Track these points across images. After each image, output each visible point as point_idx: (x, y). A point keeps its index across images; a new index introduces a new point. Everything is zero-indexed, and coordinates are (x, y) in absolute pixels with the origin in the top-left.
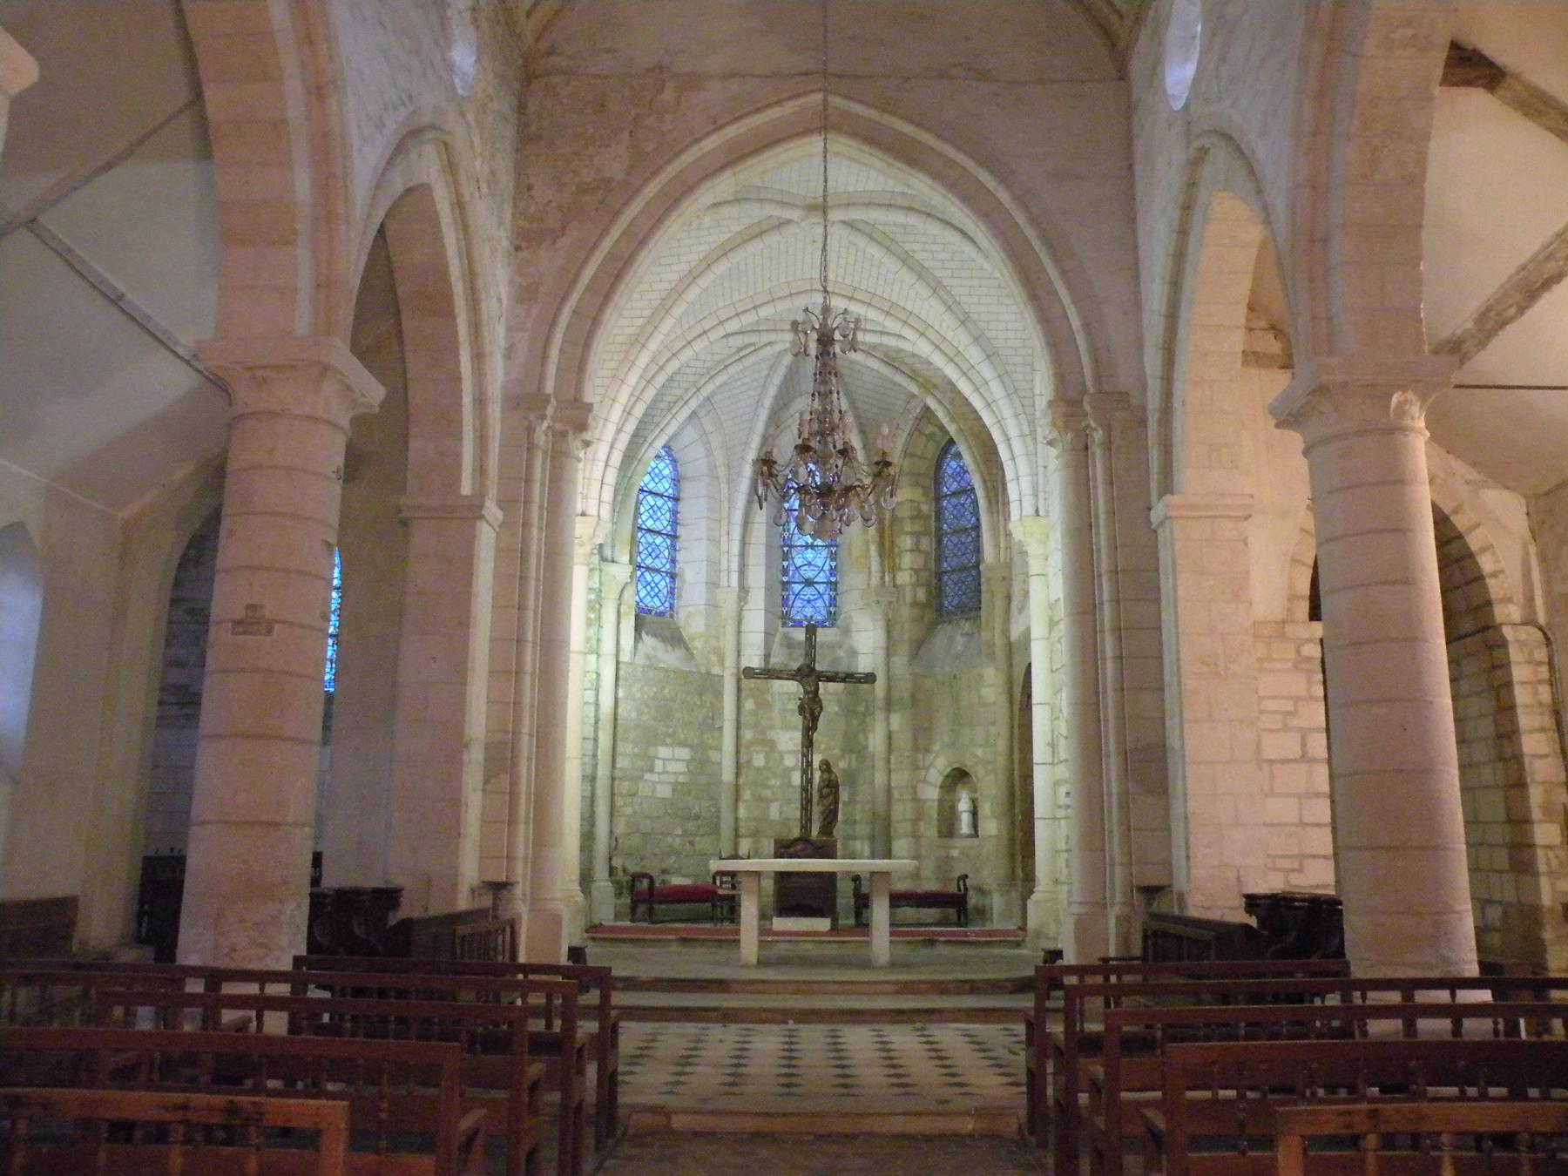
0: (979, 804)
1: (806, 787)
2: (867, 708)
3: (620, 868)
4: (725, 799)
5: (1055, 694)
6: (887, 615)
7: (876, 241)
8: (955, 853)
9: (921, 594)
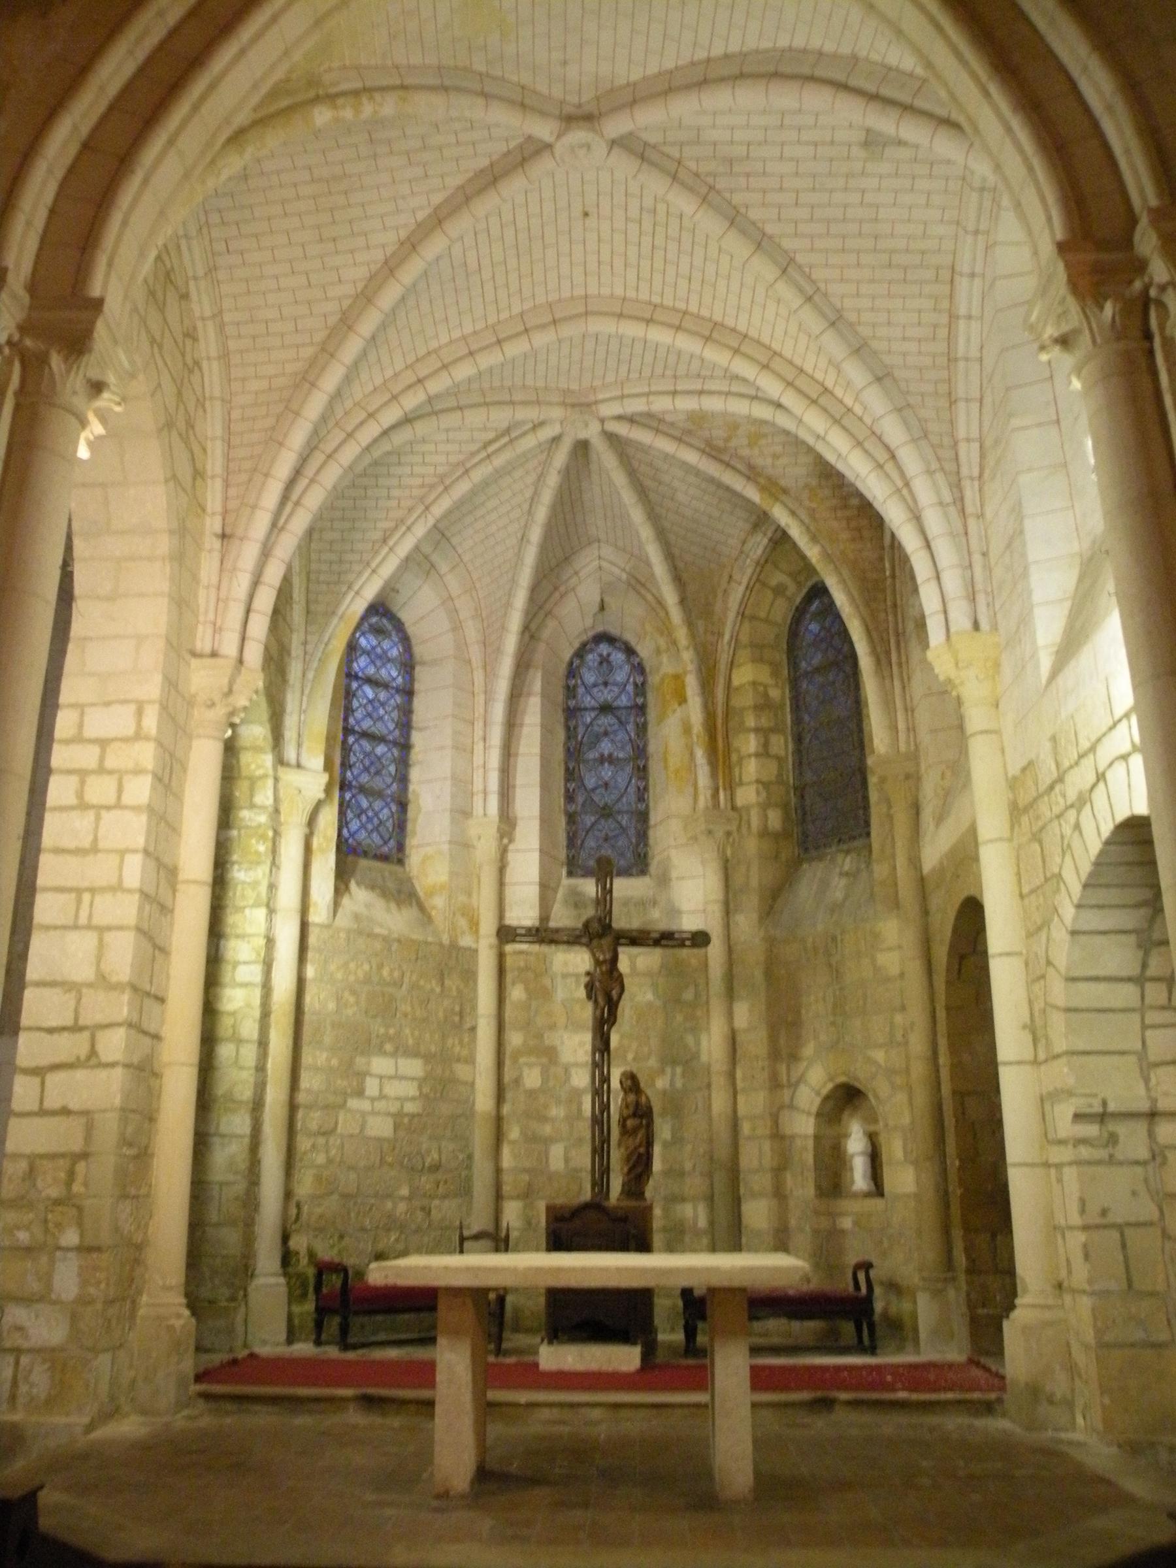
0: (882, 1139)
1: (599, 1121)
2: (697, 995)
3: (303, 1252)
4: (481, 1137)
5: (1030, 935)
6: (724, 851)
7: (683, 184)
8: (847, 1223)
9: (775, 819)
